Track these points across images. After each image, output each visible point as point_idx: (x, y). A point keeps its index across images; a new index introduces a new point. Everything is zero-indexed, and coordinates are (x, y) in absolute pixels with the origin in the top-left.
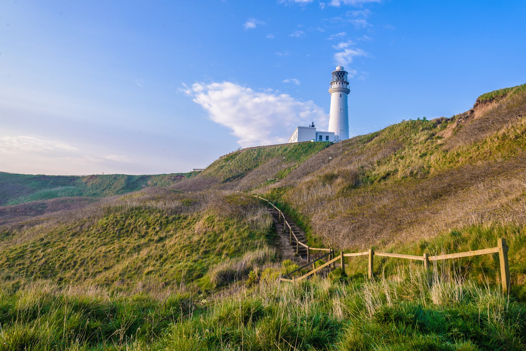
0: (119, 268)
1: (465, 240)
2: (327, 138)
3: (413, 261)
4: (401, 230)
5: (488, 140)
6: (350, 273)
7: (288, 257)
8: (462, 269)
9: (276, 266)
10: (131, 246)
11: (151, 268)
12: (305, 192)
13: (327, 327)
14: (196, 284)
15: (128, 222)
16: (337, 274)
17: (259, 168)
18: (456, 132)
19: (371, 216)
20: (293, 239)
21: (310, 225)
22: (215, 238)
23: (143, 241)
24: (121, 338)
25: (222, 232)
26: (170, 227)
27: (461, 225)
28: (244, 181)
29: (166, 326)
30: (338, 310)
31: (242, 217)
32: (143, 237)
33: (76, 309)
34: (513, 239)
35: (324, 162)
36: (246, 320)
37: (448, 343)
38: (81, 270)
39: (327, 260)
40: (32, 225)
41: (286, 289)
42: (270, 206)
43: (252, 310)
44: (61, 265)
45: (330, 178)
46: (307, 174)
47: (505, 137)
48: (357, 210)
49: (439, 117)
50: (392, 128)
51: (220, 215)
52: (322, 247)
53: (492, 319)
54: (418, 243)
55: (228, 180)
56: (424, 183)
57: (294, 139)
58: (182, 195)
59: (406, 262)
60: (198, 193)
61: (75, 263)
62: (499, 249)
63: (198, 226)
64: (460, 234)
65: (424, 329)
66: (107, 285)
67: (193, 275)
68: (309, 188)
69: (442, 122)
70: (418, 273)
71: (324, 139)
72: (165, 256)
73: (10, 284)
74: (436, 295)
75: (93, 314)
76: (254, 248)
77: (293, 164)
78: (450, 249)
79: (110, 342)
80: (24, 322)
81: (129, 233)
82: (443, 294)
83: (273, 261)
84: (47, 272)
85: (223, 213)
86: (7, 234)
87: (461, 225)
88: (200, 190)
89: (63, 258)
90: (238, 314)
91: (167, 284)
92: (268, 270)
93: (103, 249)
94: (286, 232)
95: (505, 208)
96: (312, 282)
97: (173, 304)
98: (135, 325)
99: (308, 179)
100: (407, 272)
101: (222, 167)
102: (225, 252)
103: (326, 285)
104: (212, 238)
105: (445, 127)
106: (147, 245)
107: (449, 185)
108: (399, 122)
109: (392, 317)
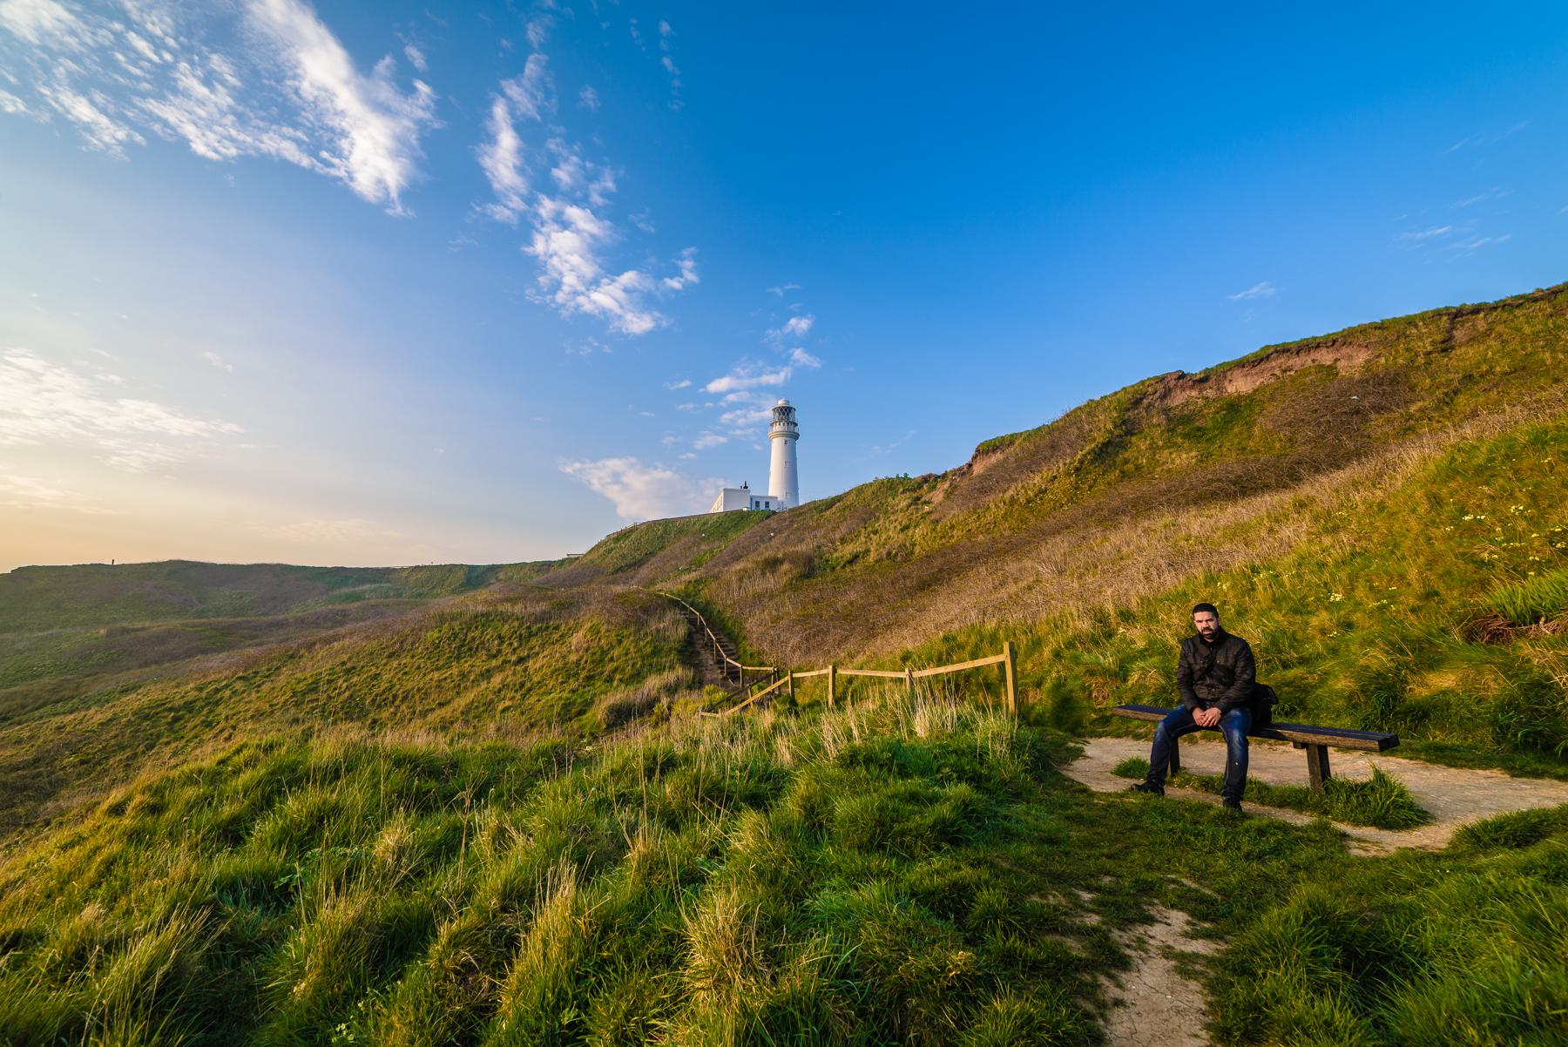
0: (461, 703)
1: (961, 647)
2: (767, 504)
3: (892, 679)
4: (874, 636)
5: (992, 505)
6: (802, 700)
7: (712, 681)
8: (959, 686)
9: (695, 695)
10: (478, 670)
11: (508, 703)
12: (735, 586)
13: (769, 779)
14: (575, 724)
15: (470, 635)
16: (783, 702)
17: (667, 552)
18: (949, 494)
19: (832, 618)
20: (719, 654)
21: (744, 633)
22: (602, 657)
23: (494, 663)
24: (468, 803)
25: (612, 647)
26: (534, 641)
27: (956, 625)
28: (644, 572)
29: (532, 785)
30: (784, 752)
31: (641, 624)
32: (495, 656)
33: (398, 763)
34: (1023, 641)
35: (763, 541)
36: (649, 773)
37: (936, 789)
38: (404, 707)
39: (769, 684)
40: (328, 641)
41: (708, 727)
42: (684, 608)
43: (659, 760)
44: (374, 701)
45: (772, 564)
46: (738, 558)
47: (1013, 501)
48: (812, 610)
49: (925, 474)
50: (860, 490)
51: (608, 623)
52: (762, 664)
53: (994, 752)
54: (898, 653)
55: (620, 569)
56: (906, 569)
57: (718, 507)
58: (549, 593)
59: (881, 681)
60: (575, 590)
61: (395, 697)
62: (1005, 657)
63: (576, 639)
64: (954, 639)
65: (904, 773)
66: (444, 728)
67: (571, 712)
68: (741, 580)
69: (930, 481)
70: (896, 696)
71: (762, 507)
72: (528, 685)
73: (298, 730)
74: (921, 726)
75: (423, 770)
76: (660, 670)
77: (717, 543)
78: (940, 662)
79: (451, 810)
80: (322, 784)
81: (473, 652)
82: (931, 722)
83: (690, 688)
84: (353, 711)
85: (613, 620)
86: (292, 657)
87: (956, 625)
88: (578, 585)
89: (376, 690)
90: (639, 764)
91: (532, 725)
92: (682, 701)
93: (436, 675)
94: (709, 645)
95: (1014, 600)
96: (748, 715)
97: (544, 753)
98: (487, 784)
99: (739, 566)
100: (882, 695)
101: (610, 551)
102: (618, 677)
103: (767, 719)
104: (597, 656)
105: (934, 487)
106: (500, 668)
107: (941, 570)
108: (871, 480)
109: (860, 758)
